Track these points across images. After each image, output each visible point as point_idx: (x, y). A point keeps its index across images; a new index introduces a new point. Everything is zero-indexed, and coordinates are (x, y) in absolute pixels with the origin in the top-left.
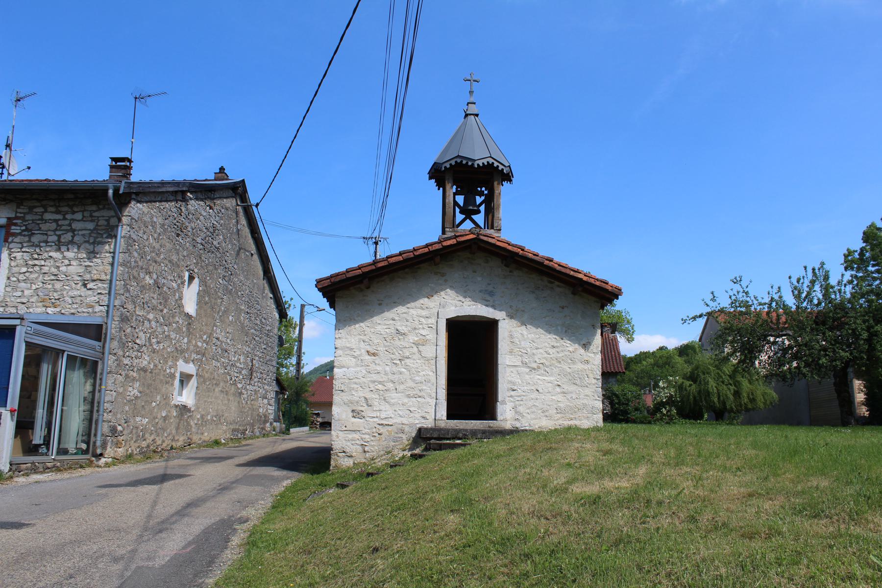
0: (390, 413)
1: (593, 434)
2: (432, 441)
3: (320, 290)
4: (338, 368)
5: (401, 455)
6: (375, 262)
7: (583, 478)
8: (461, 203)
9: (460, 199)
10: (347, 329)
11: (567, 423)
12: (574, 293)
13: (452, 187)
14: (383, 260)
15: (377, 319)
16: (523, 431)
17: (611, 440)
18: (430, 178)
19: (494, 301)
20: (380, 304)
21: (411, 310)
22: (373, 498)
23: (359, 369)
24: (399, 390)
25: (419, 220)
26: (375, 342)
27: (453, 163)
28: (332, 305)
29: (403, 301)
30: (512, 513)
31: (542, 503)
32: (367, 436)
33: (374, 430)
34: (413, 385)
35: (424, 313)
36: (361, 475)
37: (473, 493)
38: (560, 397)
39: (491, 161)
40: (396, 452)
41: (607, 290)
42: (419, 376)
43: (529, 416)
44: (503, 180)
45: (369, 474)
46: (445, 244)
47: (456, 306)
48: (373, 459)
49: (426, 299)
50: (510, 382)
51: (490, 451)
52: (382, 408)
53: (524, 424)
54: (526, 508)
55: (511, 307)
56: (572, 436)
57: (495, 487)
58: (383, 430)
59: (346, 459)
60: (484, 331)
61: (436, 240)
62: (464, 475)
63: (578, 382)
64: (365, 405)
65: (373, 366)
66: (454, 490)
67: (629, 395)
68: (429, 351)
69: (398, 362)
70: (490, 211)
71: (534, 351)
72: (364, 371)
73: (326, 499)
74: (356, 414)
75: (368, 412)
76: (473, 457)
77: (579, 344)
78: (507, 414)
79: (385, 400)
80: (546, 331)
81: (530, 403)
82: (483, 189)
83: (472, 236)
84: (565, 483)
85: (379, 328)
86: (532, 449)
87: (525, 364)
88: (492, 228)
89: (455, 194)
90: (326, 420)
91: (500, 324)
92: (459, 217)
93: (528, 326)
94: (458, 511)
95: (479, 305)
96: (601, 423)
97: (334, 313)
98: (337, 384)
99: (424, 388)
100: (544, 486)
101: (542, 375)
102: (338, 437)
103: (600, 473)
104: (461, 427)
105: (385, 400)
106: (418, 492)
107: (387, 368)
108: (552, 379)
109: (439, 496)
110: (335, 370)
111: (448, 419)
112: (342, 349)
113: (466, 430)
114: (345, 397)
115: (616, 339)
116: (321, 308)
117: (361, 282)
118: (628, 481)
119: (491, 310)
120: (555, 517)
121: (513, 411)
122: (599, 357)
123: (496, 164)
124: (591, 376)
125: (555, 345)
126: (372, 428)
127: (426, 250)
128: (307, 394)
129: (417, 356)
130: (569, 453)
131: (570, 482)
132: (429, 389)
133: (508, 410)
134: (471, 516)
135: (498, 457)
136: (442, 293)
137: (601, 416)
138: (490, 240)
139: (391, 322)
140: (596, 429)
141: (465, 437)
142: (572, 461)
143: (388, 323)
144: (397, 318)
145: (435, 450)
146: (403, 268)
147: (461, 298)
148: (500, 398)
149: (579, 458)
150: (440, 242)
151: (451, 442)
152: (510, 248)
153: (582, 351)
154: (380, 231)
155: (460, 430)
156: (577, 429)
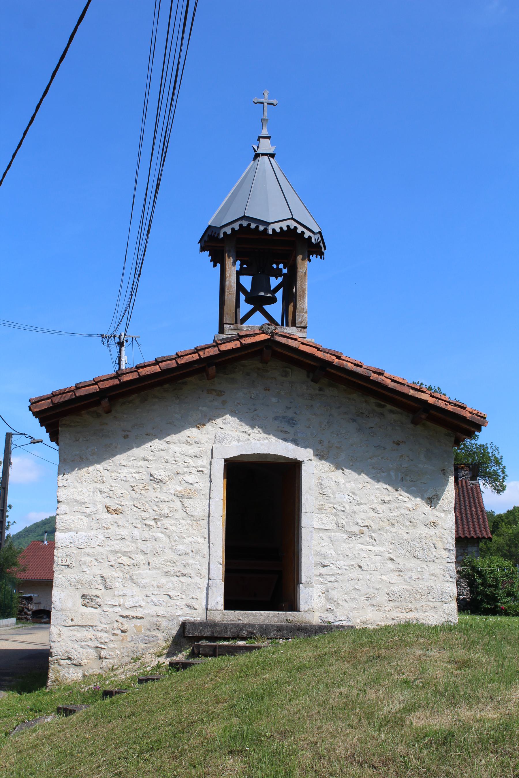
0: (139, 599)
1: (442, 635)
2: (203, 642)
3: (36, 414)
4: (62, 531)
5: (154, 664)
6: (118, 375)
7: (428, 704)
8: (248, 287)
9: (247, 281)
10: (76, 473)
11: (403, 616)
12: (415, 422)
13: (234, 264)
14: (130, 371)
15: (120, 458)
16: (338, 627)
17: (470, 645)
18: (202, 249)
19: (295, 433)
20: (126, 437)
21: (172, 446)
22: (113, 731)
23: (93, 533)
24: (152, 564)
25: (185, 313)
26: (119, 492)
27: (236, 226)
28: (54, 437)
29: (161, 433)
30: (321, 757)
31: (366, 743)
32: (104, 635)
33: (115, 625)
34: (174, 557)
35: (191, 450)
36: (94, 693)
37: (263, 726)
38: (394, 577)
39: (293, 224)
40: (147, 658)
41: (463, 419)
42: (182, 544)
43: (346, 605)
44: (311, 253)
45: (107, 694)
46: (223, 348)
47: (239, 440)
48: (113, 670)
49: (195, 430)
50: (320, 554)
51: (289, 660)
52: (128, 592)
53: (340, 617)
54: (341, 749)
55: (321, 442)
56: (410, 638)
57: (296, 716)
58: (127, 625)
59: (72, 669)
60: (284, 476)
61: (211, 342)
62: (249, 696)
63: (421, 555)
64: (101, 587)
65: (114, 529)
66: (235, 720)
67: (498, 572)
68: (198, 507)
69: (152, 523)
70: (291, 298)
71: (356, 508)
72: (101, 537)
73: (40, 732)
74: (88, 600)
75: (105, 598)
76: (263, 668)
77: (422, 498)
78: (314, 602)
79: (132, 579)
80: (373, 478)
81: (349, 586)
82: (281, 266)
83: (263, 337)
84: (400, 711)
85: (124, 472)
86: (351, 657)
87: (341, 527)
88: (294, 324)
89: (239, 274)
90: (42, 607)
91: (305, 468)
92: (245, 308)
93: (346, 471)
94: (240, 752)
95: (274, 439)
96: (455, 617)
97: (57, 448)
98: (59, 555)
99: (191, 561)
100: (370, 716)
101: (367, 544)
102: (60, 635)
103: (452, 696)
104: (246, 621)
105: (132, 579)
106: (180, 722)
107: (136, 532)
108: (381, 549)
109: (214, 729)
110: (58, 535)
111: (225, 609)
112: (68, 504)
113: (253, 626)
114: (72, 575)
115: (478, 488)
116: (37, 438)
117: (98, 403)
118: (496, 709)
119: (291, 446)
120: (385, 763)
121: (323, 598)
122: (452, 517)
123: (300, 229)
124: (440, 545)
125: (387, 498)
126: (112, 622)
127: (196, 357)
128: (14, 569)
129: (181, 514)
130: (407, 664)
131: (408, 710)
132: (197, 564)
133: (315, 596)
134: (259, 760)
135: (300, 669)
136: (219, 421)
137: (454, 605)
138: (291, 343)
139: (143, 463)
140: (447, 628)
141: (251, 636)
142: (411, 677)
143: (135, 463)
144: (151, 458)
145: (206, 656)
146: (160, 384)
147: (247, 428)
148: (304, 577)
149: (421, 672)
150: (216, 345)
151: (230, 643)
152: (319, 354)
153: (426, 508)
154: (127, 327)
155: (244, 626)
156: (420, 626)
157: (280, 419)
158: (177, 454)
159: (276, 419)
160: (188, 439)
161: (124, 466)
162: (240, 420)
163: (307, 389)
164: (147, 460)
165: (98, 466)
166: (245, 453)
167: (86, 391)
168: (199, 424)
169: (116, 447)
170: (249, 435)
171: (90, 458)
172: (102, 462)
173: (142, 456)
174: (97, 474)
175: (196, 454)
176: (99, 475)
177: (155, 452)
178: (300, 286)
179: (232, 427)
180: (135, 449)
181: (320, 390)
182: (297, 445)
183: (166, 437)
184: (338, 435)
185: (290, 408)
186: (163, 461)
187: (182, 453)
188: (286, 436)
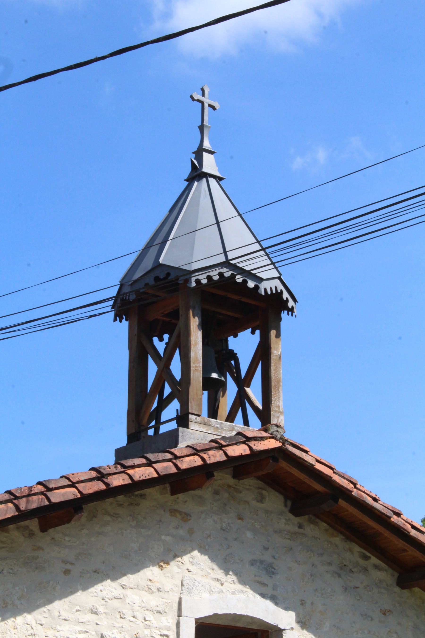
15: (59, 606)
20: (67, 572)
21: (128, 592)
27: (215, 274)
29: (114, 570)
35: (154, 601)
39: (280, 287)
47: (211, 592)
119: (269, 604)
136: (186, 558)
139: (89, 617)
144: (101, 609)
147: (219, 573)
152: (336, 478)
157: (258, 564)
158: (136, 607)
159: (253, 563)
160: (149, 583)
161: (65, 620)
162: (212, 559)
163: (286, 524)
164: (96, 613)
165: (29, 617)
166: (220, 612)
167: (63, 495)
168: (162, 561)
169: (54, 588)
170: (222, 584)
171: (17, 602)
172: (34, 610)
173: (90, 606)
174: (27, 630)
175: (159, 609)
176: (29, 633)
177: (107, 600)
178: (275, 373)
179: (202, 570)
180: (80, 593)
181: (300, 526)
182: (277, 604)
183: (120, 577)
184: (322, 594)
185: (324, 553)
186: (118, 616)
187: (143, 605)
188: (265, 590)
